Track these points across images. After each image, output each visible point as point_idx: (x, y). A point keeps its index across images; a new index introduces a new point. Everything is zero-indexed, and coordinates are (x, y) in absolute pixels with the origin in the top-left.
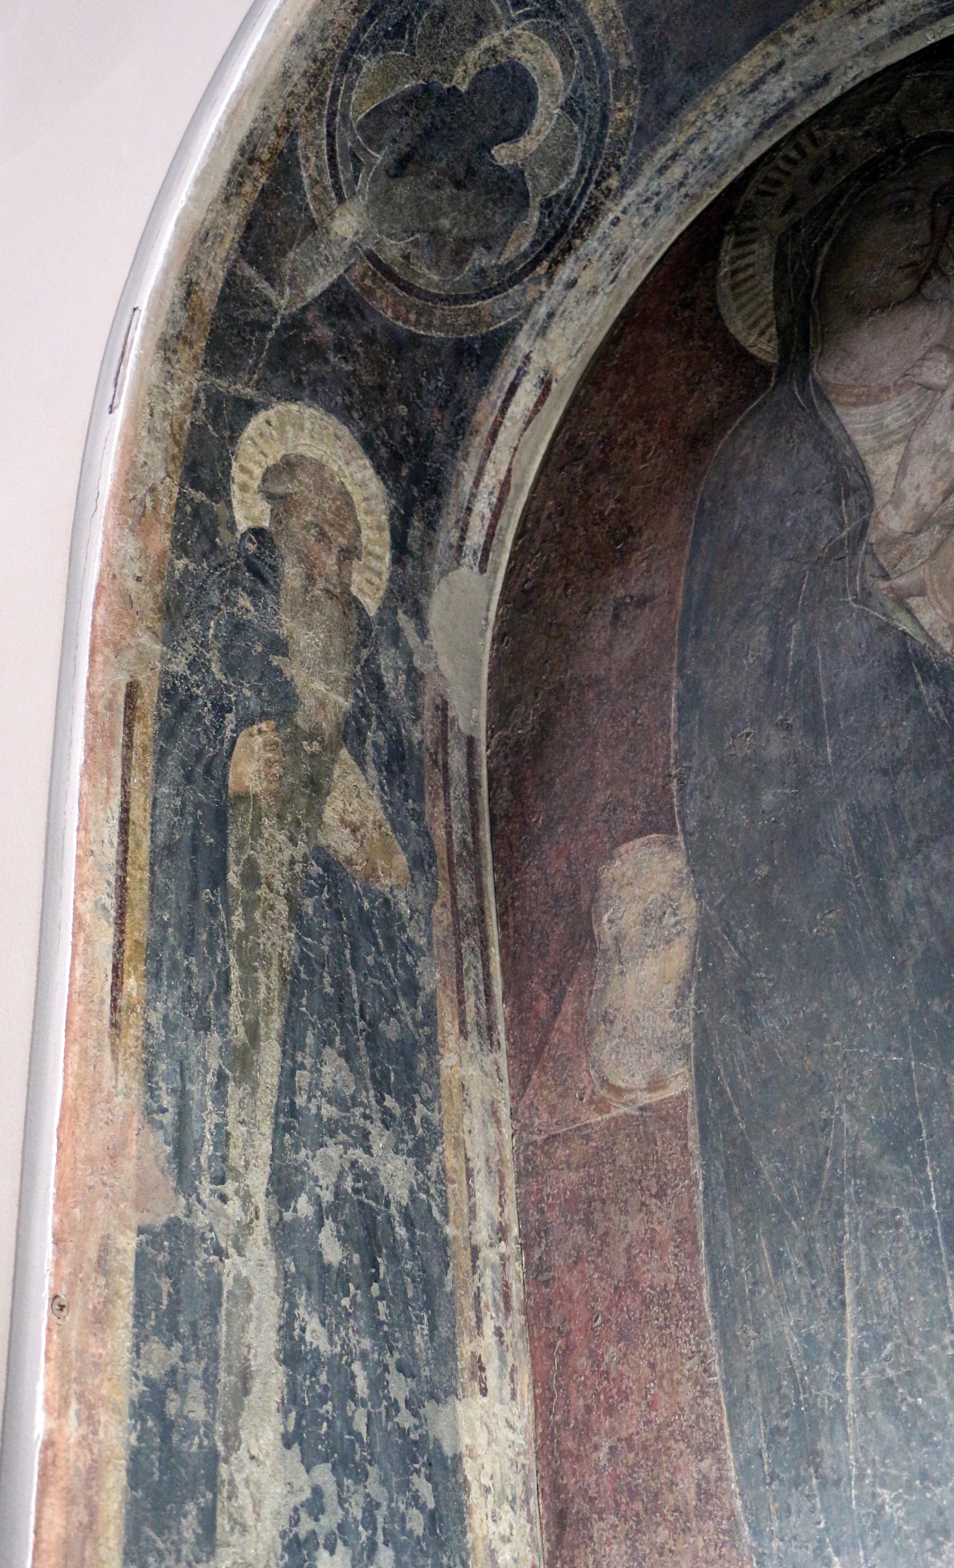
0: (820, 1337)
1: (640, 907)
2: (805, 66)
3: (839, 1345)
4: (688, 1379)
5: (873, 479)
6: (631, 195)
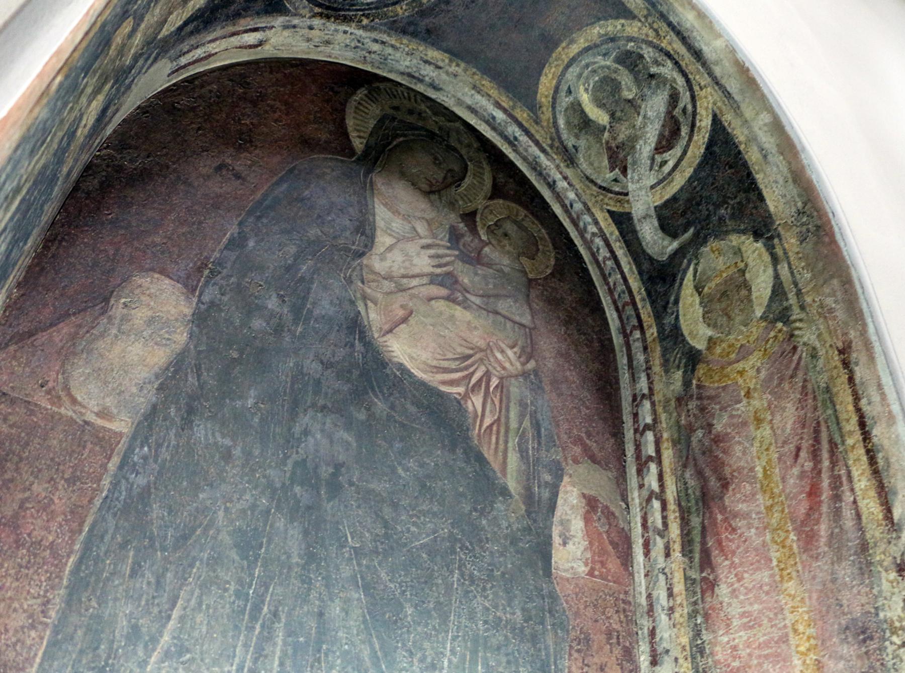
0: (144, 630)
1: (150, 313)
2: (439, 77)
3: (154, 640)
4: (24, 611)
5: (377, 240)
6: (360, 32)
